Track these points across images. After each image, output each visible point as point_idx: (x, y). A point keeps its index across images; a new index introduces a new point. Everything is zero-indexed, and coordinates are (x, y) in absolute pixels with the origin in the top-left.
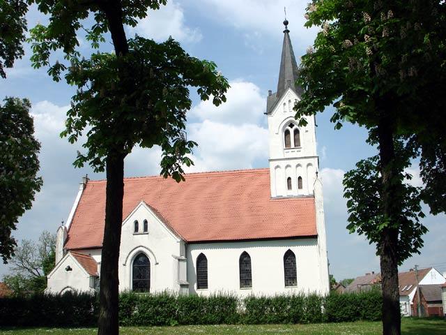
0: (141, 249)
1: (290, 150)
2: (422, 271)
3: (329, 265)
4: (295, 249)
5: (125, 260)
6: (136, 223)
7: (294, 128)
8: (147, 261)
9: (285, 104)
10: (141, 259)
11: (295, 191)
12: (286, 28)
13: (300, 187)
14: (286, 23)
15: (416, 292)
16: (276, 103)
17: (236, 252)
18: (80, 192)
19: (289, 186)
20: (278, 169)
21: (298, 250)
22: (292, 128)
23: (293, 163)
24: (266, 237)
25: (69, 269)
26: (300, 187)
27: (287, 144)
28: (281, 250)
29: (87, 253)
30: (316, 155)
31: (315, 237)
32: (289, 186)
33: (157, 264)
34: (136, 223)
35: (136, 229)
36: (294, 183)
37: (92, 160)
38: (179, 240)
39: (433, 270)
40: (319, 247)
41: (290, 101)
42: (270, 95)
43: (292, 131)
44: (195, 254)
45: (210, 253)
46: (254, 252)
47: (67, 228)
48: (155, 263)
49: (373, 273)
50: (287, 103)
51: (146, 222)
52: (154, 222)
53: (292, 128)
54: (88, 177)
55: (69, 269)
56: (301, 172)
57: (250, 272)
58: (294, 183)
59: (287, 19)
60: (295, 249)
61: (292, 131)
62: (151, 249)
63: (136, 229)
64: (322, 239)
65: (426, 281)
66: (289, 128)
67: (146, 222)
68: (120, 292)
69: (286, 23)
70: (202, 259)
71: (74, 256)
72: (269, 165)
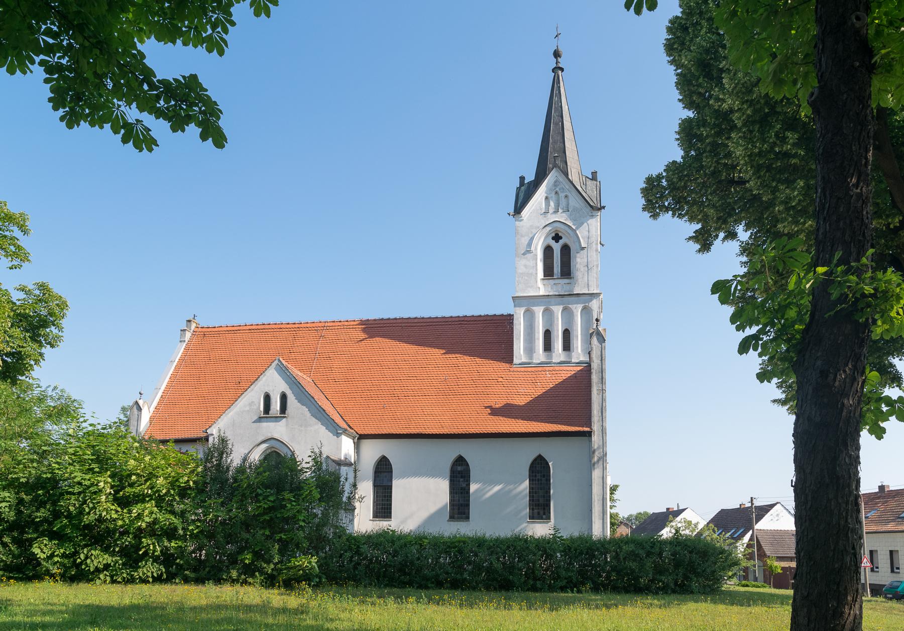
6: (267, 398)
7: (561, 242)
22: (557, 241)
34: (267, 398)
39: (778, 507)
69: (557, 54)
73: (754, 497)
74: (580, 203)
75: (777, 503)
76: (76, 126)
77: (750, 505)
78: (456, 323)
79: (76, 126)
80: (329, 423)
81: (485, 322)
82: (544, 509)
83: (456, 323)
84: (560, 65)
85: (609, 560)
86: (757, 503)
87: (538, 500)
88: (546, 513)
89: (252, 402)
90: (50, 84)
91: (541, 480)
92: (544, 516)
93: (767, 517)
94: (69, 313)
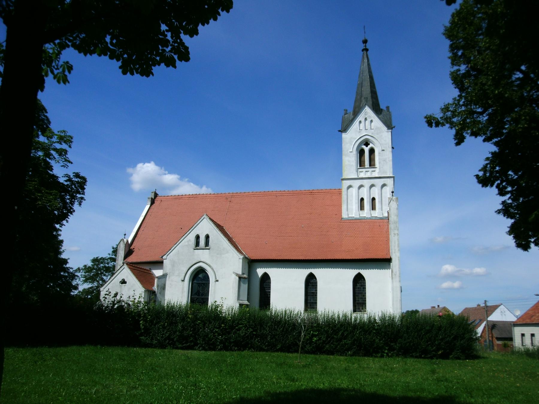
0: (201, 264)
1: (364, 170)
2: (491, 307)
3: (401, 291)
4: (365, 273)
5: (184, 275)
6: (198, 237)
7: (369, 147)
8: (206, 278)
9: (360, 122)
10: (201, 276)
11: (367, 213)
12: (366, 46)
13: (373, 208)
14: (365, 42)
15: (485, 327)
16: (352, 121)
17: (302, 273)
18: (148, 207)
19: (362, 208)
20: (362, 188)
21: (367, 273)
22: (367, 146)
23: (367, 183)
24: (379, 257)
25: (123, 282)
26: (373, 208)
27: (361, 164)
28: (350, 273)
29: (147, 267)
30: (391, 175)
31: (162, 262)
32: (362, 208)
33: (217, 281)
34: (198, 237)
35: (197, 244)
36: (367, 204)
37: (48, 159)
38: (242, 257)
39: (502, 307)
40: (392, 272)
41: (366, 119)
42: (346, 114)
43: (367, 149)
44: (260, 272)
45: (274, 273)
46: (320, 273)
47: (130, 242)
48: (214, 280)
49: (438, 306)
50: (363, 120)
51: (207, 237)
52: (216, 236)
53: (367, 146)
54: (157, 192)
55: (123, 282)
56: (375, 192)
57: (316, 295)
58: (367, 204)
59: (367, 38)
60: (365, 273)
61: (367, 149)
62: (211, 265)
63: (197, 244)
64: (395, 263)
65: (495, 317)
66: (364, 147)
67: (207, 237)
68: (210, 304)
69: (365, 42)
70: (266, 278)
71: (130, 268)
72: (341, 184)
73: (487, 300)
74: (380, 124)
75: (502, 304)
76: (218, 16)
77: (484, 305)
78: (308, 194)
79: (218, 16)
80: (234, 253)
81: (324, 193)
82: (362, 306)
83: (308, 194)
84: (367, 47)
85: (522, 126)
86: (489, 304)
87: (359, 301)
88: (364, 308)
89: (189, 240)
90: (109, 43)
91: (360, 288)
92: (362, 310)
93: (498, 311)
94: (87, 183)
